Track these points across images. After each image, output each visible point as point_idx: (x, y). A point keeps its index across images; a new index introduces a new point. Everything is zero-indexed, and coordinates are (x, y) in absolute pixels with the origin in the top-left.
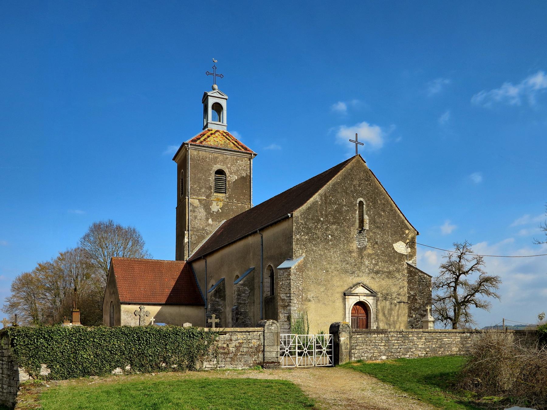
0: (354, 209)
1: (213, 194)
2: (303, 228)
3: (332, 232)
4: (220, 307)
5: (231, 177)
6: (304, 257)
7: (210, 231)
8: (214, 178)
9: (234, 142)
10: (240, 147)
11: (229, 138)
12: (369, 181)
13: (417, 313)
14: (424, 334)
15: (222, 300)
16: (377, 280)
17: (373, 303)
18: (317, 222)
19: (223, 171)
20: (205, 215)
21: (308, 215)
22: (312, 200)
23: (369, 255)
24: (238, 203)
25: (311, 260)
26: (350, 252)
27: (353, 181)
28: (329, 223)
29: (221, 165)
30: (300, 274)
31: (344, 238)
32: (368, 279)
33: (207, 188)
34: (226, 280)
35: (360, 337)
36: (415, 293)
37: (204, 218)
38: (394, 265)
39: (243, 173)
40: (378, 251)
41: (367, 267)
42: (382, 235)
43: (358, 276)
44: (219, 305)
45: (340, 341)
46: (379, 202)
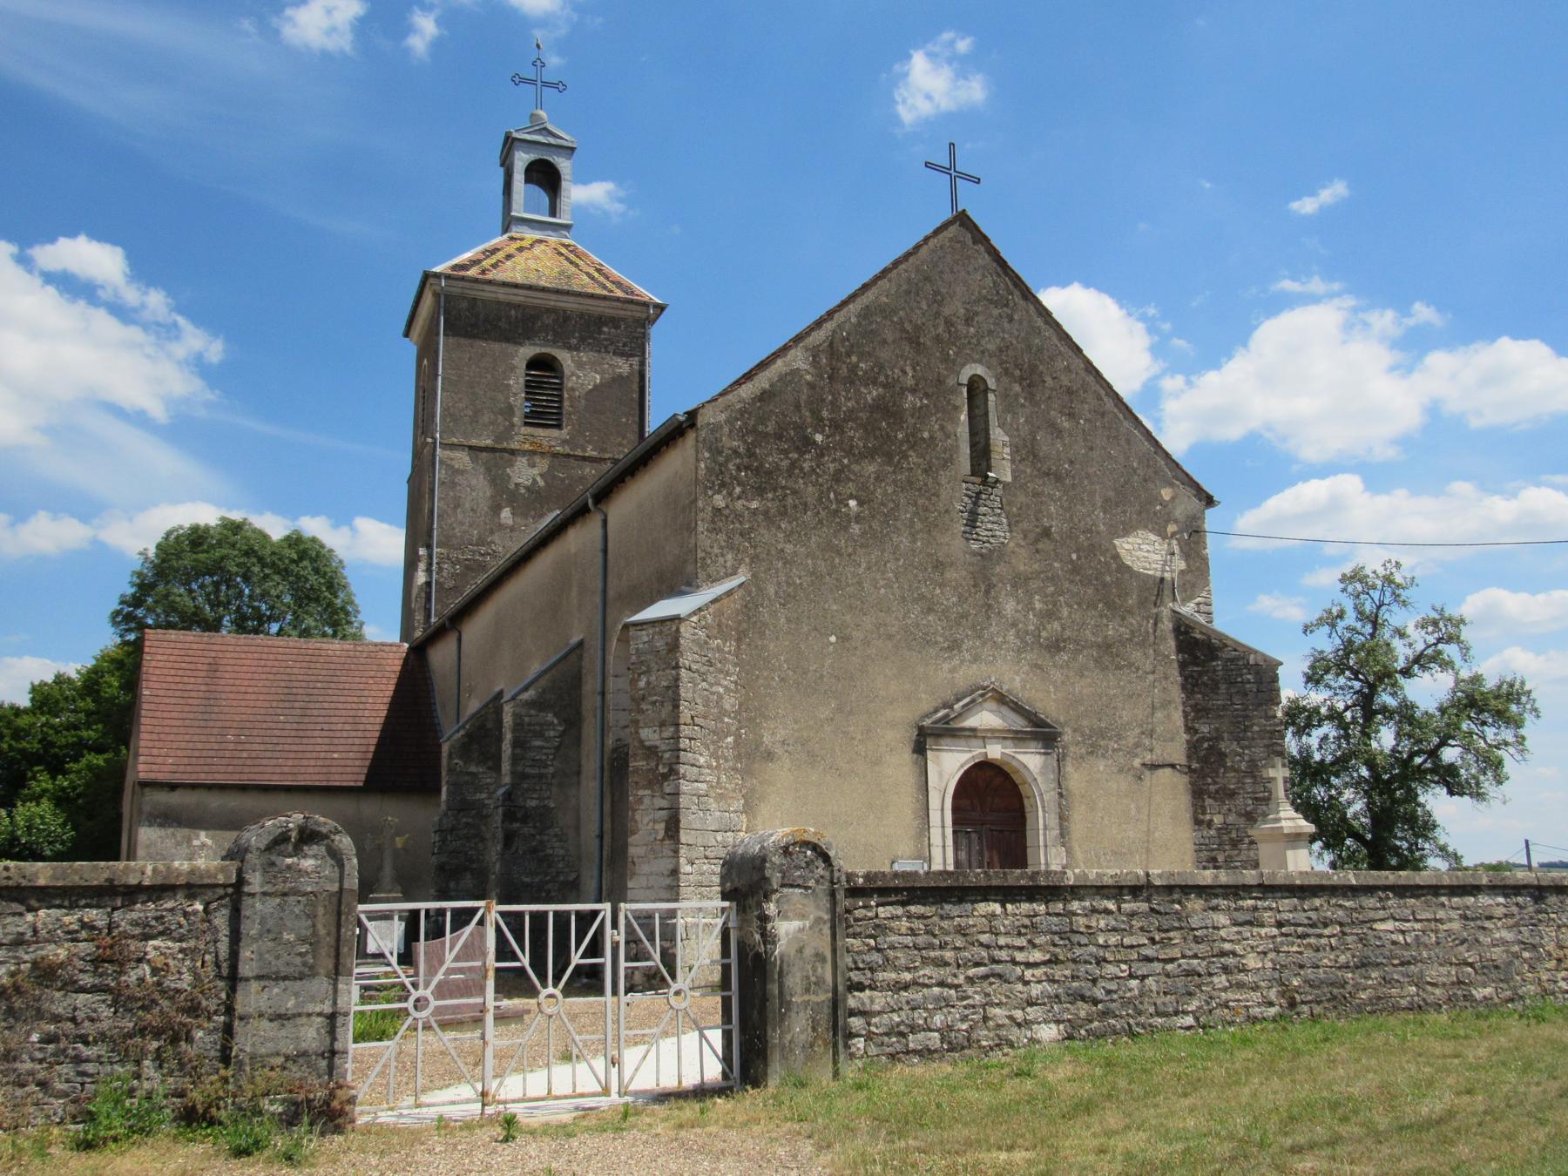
2: (739, 469)
3: (864, 487)
4: (484, 796)
5: (579, 377)
8: (522, 381)
9: (592, 271)
12: (1006, 305)
15: (489, 768)
16: (1057, 675)
17: (1044, 767)
18: (797, 449)
21: (763, 420)
25: (776, 592)
26: (939, 566)
27: (940, 303)
28: (849, 452)
30: (726, 649)
31: (912, 509)
32: (1017, 673)
33: (501, 412)
36: (1217, 729)
37: (484, 507)
38: (1123, 619)
41: (1014, 625)
42: (1066, 504)
43: (976, 659)
44: (479, 789)
45: (774, 943)
46: (1049, 382)
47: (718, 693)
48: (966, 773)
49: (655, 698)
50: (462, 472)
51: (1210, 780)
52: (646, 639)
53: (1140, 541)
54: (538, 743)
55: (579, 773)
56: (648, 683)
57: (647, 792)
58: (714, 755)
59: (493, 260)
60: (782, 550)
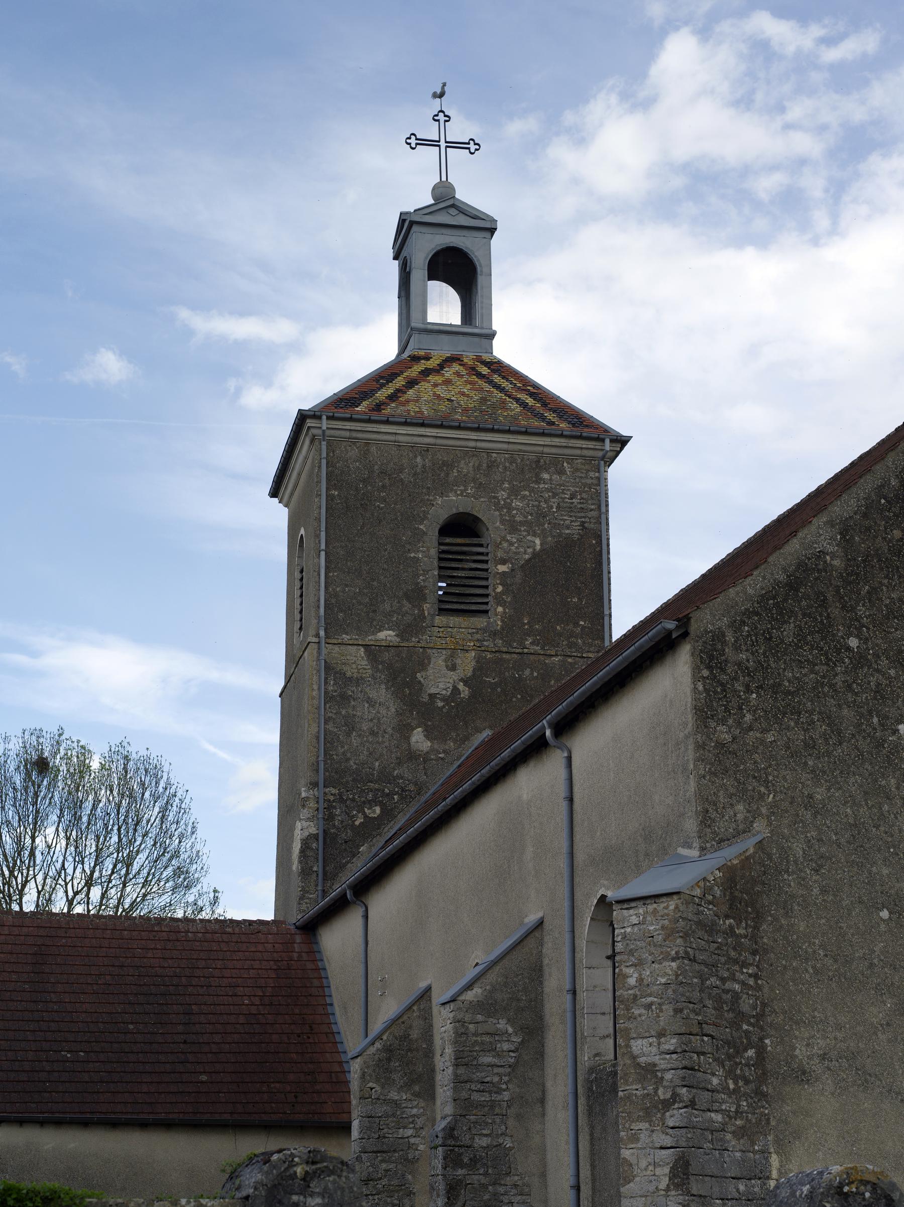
1: (433, 620)
4: (409, 1132)
6: (759, 838)
7: (416, 784)
8: (433, 552)
9: (522, 396)
10: (550, 416)
11: (505, 384)
15: (417, 1095)
19: (477, 520)
20: (393, 710)
29: (468, 496)
39: (568, 522)
47: (734, 991)
49: (650, 999)
50: (358, 681)
52: (634, 920)
54: (487, 1059)
55: (542, 1101)
56: (640, 980)
57: (644, 1125)
58: (730, 1074)
59: (389, 390)
60: (810, 796)
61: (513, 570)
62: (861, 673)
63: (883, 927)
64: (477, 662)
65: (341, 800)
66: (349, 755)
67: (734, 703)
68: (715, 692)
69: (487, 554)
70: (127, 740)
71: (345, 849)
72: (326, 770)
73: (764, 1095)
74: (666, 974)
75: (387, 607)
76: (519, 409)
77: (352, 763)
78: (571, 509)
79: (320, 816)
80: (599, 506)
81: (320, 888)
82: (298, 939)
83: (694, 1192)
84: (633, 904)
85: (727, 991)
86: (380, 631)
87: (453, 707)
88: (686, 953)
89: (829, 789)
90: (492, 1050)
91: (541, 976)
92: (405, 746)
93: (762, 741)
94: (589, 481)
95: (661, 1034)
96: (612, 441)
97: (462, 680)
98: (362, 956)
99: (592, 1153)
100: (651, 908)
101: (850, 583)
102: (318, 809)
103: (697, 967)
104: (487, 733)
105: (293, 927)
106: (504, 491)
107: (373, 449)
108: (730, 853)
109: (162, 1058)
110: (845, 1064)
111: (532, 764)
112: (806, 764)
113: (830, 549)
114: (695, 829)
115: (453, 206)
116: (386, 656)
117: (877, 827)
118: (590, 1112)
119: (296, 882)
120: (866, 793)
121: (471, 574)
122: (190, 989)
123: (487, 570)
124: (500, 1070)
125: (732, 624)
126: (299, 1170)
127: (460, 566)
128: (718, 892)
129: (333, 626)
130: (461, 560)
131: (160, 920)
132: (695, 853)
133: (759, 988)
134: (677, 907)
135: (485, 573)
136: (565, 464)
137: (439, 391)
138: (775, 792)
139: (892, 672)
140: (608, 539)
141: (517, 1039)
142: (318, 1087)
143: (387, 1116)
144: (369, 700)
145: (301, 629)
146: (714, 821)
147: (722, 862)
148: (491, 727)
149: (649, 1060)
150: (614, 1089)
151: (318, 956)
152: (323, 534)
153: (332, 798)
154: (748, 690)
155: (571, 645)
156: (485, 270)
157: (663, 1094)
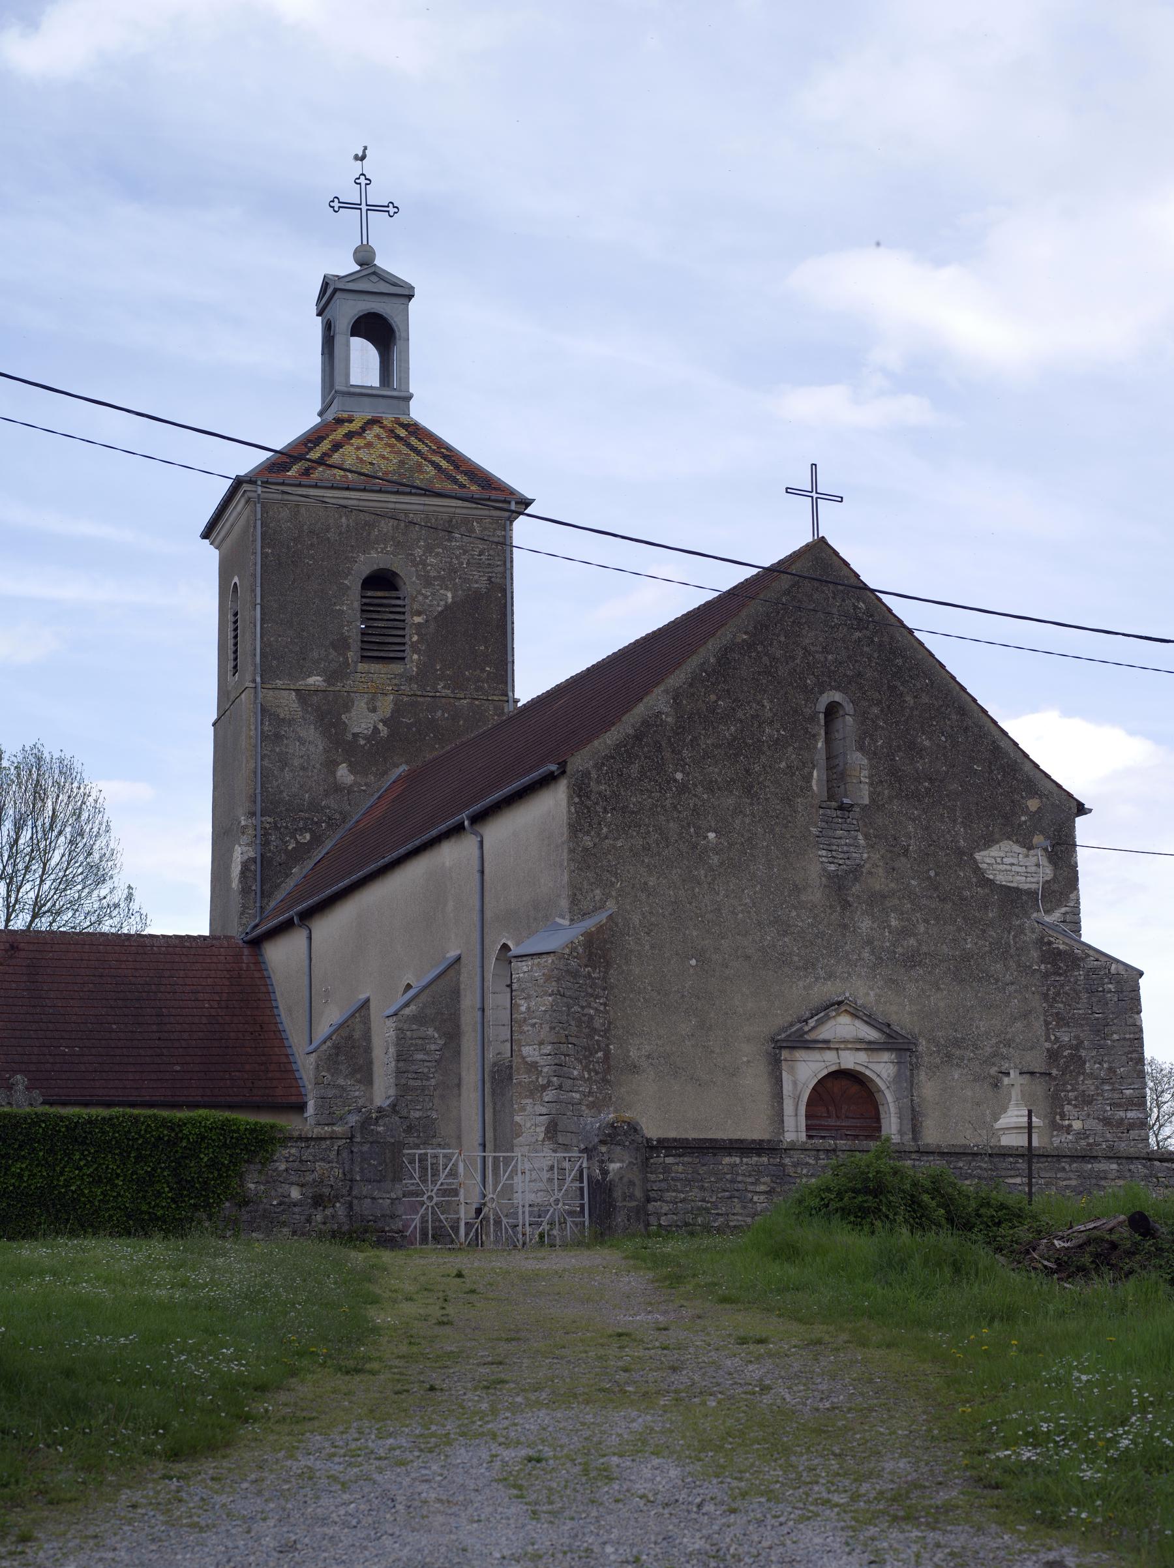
0: (807, 732)
1: (356, 667)
6: (610, 912)
8: (357, 605)
9: (437, 459)
10: (461, 478)
11: (421, 446)
13: (1089, 1115)
14: (925, 1158)
15: (359, 1082)
19: (395, 574)
20: (321, 748)
22: (640, 710)
23: (875, 899)
24: (458, 696)
26: (797, 889)
32: (872, 989)
33: (334, 645)
34: (373, 1004)
35: (677, 1164)
40: (913, 882)
41: (869, 942)
43: (830, 976)
47: (590, 1015)
48: (821, 1082)
49: (534, 1021)
50: (290, 722)
51: (1069, 1087)
52: (525, 969)
53: (1002, 855)
54: (420, 1056)
55: (459, 1085)
56: (528, 1008)
57: (529, 1101)
58: (586, 1068)
60: (646, 883)
61: (427, 621)
62: (683, 797)
63: (691, 970)
64: (395, 704)
65: (276, 828)
66: (282, 788)
67: (595, 821)
68: (583, 813)
69: (404, 606)
70: (41, 742)
71: (280, 871)
72: (262, 801)
73: (608, 1082)
74: (546, 1005)
75: (315, 655)
76: (433, 473)
77: (285, 794)
78: (479, 565)
79: (258, 842)
80: (505, 564)
81: (258, 905)
82: (246, 952)
83: (560, 1142)
84: (524, 959)
85: (585, 1015)
86: (309, 676)
87: (373, 745)
88: (559, 991)
89: (658, 878)
90: (423, 1050)
91: (459, 997)
92: (331, 779)
93: (614, 847)
94: (496, 539)
95: (541, 1043)
96: (517, 503)
97: (381, 721)
98: (306, 969)
99: (495, 1121)
100: (536, 961)
101: (678, 734)
102: (255, 836)
103: (565, 1000)
104: (404, 768)
105: (240, 942)
106: (420, 548)
107: (303, 510)
108: (589, 924)
109: (142, 1052)
110: (663, 1061)
111: (453, 840)
112: (643, 861)
113: (665, 710)
114: (567, 906)
115: (374, 273)
116: (315, 699)
117: (690, 903)
118: (493, 1093)
119: (236, 900)
120: (684, 880)
121: (390, 624)
122: (159, 995)
123: (404, 621)
124: (428, 1064)
125: (595, 765)
126: (374, 1116)
127: (380, 617)
128: (580, 950)
129: (269, 669)
130: (379, 612)
131: (117, 936)
132: (567, 923)
133: (607, 1012)
134: (553, 961)
135: (402, 623)
136: (475, 524)
137: (362, 454)
138: (622, 881)
139: (705, 796)
140: (512, 592)
141: (442, 1042)
142: (270, 1075)
143: (336, 1097)
144: (300, 739)
145: (235, 667)
146: (579, 901)
147: (583, 930)
148: (407, 763)
149: (533, 1059)
150: (510, 1078)
151: (263, 966)
152: (258, 589)
153: (268, 826)
154: (605, 811)
155: (477, 689)
156: (403, 335)
157: (542, 1081)
